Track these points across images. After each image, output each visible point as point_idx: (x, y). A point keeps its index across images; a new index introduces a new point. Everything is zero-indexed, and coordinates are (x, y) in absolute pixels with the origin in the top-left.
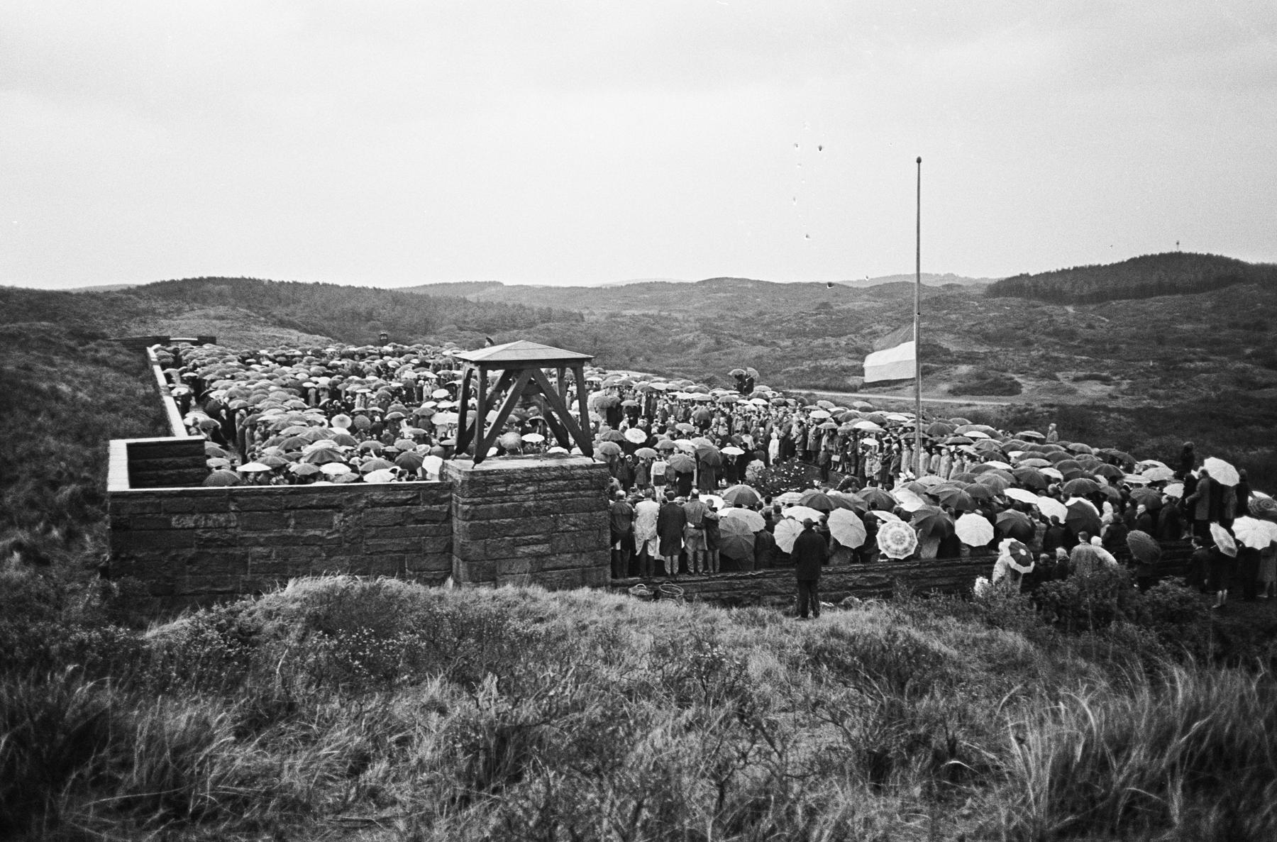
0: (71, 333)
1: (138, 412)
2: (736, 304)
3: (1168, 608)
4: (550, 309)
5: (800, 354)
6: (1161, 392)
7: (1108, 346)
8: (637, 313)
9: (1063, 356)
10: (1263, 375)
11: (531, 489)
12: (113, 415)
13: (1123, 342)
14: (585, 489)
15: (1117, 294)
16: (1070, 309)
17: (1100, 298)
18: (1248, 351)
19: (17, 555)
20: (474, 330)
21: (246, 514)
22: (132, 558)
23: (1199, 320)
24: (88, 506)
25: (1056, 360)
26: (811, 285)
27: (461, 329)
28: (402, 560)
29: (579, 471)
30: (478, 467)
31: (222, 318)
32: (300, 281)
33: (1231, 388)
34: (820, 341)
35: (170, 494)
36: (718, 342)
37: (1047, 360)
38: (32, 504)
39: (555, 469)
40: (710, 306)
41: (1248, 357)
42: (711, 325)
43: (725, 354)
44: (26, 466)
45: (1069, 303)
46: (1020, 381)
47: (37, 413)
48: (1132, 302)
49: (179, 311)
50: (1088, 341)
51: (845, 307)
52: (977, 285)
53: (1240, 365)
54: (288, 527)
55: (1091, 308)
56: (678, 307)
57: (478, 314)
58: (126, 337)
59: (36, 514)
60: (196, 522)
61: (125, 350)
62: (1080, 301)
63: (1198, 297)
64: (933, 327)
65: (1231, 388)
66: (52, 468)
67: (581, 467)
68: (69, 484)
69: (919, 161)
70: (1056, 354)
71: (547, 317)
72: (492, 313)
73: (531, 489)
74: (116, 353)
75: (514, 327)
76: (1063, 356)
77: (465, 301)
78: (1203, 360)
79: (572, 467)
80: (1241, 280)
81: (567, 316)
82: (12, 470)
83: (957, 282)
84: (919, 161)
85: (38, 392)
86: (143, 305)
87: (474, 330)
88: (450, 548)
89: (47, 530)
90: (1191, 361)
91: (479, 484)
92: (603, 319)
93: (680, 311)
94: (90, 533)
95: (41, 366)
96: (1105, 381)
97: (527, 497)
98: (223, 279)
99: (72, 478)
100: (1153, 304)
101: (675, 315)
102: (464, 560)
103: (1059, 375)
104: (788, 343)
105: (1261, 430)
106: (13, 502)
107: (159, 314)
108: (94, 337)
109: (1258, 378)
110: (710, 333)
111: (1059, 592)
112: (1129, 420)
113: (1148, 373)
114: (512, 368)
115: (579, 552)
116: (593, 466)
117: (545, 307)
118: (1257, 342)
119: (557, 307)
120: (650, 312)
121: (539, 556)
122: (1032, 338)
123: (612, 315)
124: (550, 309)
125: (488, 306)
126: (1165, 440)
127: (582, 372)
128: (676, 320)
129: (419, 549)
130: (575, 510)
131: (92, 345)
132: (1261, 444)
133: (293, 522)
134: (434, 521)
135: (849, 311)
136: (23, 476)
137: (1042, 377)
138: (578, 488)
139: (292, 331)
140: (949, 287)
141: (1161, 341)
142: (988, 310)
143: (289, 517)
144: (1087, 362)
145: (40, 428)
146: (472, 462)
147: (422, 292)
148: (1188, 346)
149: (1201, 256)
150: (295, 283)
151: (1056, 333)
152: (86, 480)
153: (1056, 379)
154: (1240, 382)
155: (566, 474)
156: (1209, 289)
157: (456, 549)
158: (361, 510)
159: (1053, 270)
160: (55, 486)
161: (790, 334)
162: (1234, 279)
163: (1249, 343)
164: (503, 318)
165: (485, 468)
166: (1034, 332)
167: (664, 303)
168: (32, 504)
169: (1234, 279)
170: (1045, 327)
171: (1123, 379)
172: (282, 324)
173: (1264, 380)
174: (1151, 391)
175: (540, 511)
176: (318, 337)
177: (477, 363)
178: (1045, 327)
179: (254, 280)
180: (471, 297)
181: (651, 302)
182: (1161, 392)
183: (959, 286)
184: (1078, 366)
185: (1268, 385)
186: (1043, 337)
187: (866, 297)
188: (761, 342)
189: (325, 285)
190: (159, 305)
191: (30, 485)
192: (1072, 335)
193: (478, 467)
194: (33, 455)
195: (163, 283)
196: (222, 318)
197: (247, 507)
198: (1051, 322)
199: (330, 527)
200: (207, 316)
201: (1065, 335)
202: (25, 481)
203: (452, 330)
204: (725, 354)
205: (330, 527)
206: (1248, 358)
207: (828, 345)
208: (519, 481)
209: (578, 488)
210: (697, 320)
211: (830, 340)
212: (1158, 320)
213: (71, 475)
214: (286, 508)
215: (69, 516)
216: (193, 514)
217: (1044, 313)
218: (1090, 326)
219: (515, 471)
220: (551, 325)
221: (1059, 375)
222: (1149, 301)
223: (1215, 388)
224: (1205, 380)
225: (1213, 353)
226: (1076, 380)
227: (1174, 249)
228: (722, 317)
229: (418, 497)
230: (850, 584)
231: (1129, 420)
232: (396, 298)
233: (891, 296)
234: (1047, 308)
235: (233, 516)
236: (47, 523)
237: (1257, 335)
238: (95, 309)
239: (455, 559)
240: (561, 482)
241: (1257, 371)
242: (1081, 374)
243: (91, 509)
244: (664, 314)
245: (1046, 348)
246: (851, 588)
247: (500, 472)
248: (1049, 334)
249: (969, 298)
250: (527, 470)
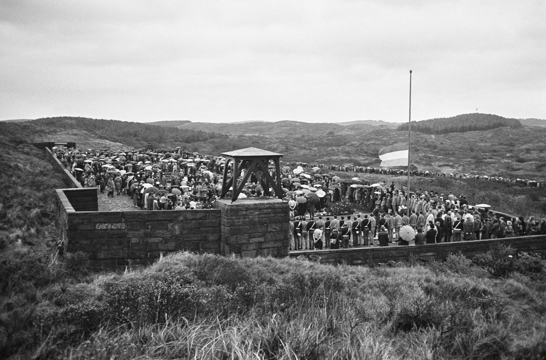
0: (11, 140)
1: (56, 176)
2: (292, 132)
3: (530, 266)
4: (213, 133)
5: (322, 153)
6: (475, 171)
7: (450, 152)
8: (250, 135)
9: (432, 156)
10: (516, 165)
11: (257, 213)
12: (46, 178)
13: (456, 150)
14: (280, 213)
15: (452, 130)
16: (433, 136)
17: (446, 131)
18: (508, 155)
19: (20, 240)
20: (181, 141)
21: (129, 223)
22: (78, 243)
23: (486, 142)
24: (43, 218)
25: (430, 158)
26: (323, 124)
27: (175, 141)
28: (198, 244)
29: (277, 205)
30: (234, 203)
31: (75, 135)
32: (104, 119)
33: (504, 171)
34: (330, 148)
35: (533, 238)
36: (287, 148)
37: (426, 157)
38: (19, 217)
39: (267, 204)
40: (281, 133)
41: (509, 158)
42: (283, 141)
43: (291, 153)
44: (15, 200)
45: (432, 133)
46: (417, 166)
47: (11, 176)
48: (459, 134)
49: (55, 132)
50: (442, 150)
51: (339, 134)
52: (393, 125)
53: (506, 161)
54: (148, 229)
55: (442, 136)
56: (267, 133)
57: (182, 135)
58: (34, 142)
59: (22, 222)
60: (107, 226)
61: (35, 148)
62: (437, 133)
63: (485, 132)
64: (377, 143)
65: (504, 171)
66: (27, 202)
67: (278, 203)
68: (35, 208)
69: (411, 72)
70: (429, 155)
71: (212, 136)
72: (188, 134)
73: (257, 213)
74: (32, 149)
75: (198, 141)
76: (432, 156)
77: (176, 129)
78: (491, 158)
79: (274, 203)
80: (504, 125)
81: (221, 136)
82: (9, 202)
83: (384, 124)
84: (411, 72)
85: (10, 167)
86: (38, 128)
87: (181, 141)
88: (220, 239)
89: (28, 229)
90: (485, 159)
91: (235, 211)
92: (236, 137)
93: (268, 135)
94: (47, 230)
95: (5, 155)
96: (452, 166)
97: (255, 216)
98: (70, 117)
99: (36, 206)
100: (468, 135)
101: (266, 136)
102: (227, 244)
103: (433, 164)
104: (315, 149)
105: (519, 188)
106: (12, 216)
107: (46, 133)
108: (21, 142)
109: (515, 166)
110: (283, 144)
111: (484, 259)
112: (465, 183)
113: (470, 163)
114: (247, 161)
115: (276, 241)
116: (283, 203)
117: (211, 132)
118: (511, 151)
119: (217, 132)
120: (256, 135)
121: (260, 243)
122: (418, 148)
123: (240, 136)
124: (213, 133)
125: (187, 131)
126: (488, 192)
127: (278, 161)
128: (267, 138)
129: (206, 240)
130: (275, 222)
131: (21, 146)
132: (520, 194)
133: (150, 227)
134: (213, 227)
135: (341, 135)
136: (15, 205)
137: (426, 165)
138: (277, 212)
139: (107, 141)
140: (382, 126)
141: (472, 150)
142: (399, 136)
143: (149, 225)
144: (443, 159)
145: (14, 183)
146: (231, 201)
147: (157, 125)
148: (483, 152)
149: (487, 115)
150: (102, 120)
151: (429, 146)
152: (42, 207)
153: (432, 166)
154: (508, 168)
155: (272, 207)
156: (490, 129)
157: (223, 239)
158: (182, 221)
159: (426, 119)
160: (29, 209)
161: (316, 146)
162: (500, 125)
163: (508, 151)
164: (193, 136)
165: (237, 204)
166: (419, 146)
167: (261, 131)
168: (19, 217)
169: (500, 125)
170: (424, 144)
171: (459, 166)
172: (101, 137)
173: (518, 167)
174: (471, 171)
175: (262, 223)
176: (118, 143)
177: (234, 157)
178: (424, 144)
179: (84, 118)
180: (178, 127)
181: (256, 131)
182: (475, 171)
183: (386, 126)
184: (439, 160)
185: (518, 170)
186: (423, 148)
187: (347, 130)
188: (305, 148)
189: (115, 121)
190: (45, 128)
191: (18, 208)
192: (435, 147)
193: (234, 203)
194: (16, 195)
195: (43, 119)
196: (75, 135)
197: (130, 220)
198: (426, 141)
199: (167, 229)
200: (68, 134)
201: (432, 147)
202: (16, 207)
203: (172, 141)
204: (291, 153)
205: (167, 229)
206: (509, 158)
207: (333, 150)
208: (252, 209)
209: (277, 212)
210: (276, 138)
211: (335, 148)
212: (470, 141)
213: (35, 204)
214: (148, 221)
215: (36, 223)
216: (105, 223)
217: (422, 138)
218: (442, 144)
219: (249, 205)
220: (215, 140)
221: (433, 164)
222: (465, 133)
223: (497, 170)
224: (493, 167)
225: (494, 155)
226: (440, 166)
227: (476, 112)
228: (286, 138)
229: (206, 216)
230: (390, 255)
231: (465, 183)
232: (147, 127)
233: (357, 129)
234: (424, 135)
235: (124, 225)
236: (28, 226)
237: (511, 148)
238: (17, 130)
239: (222, 244)
240: (269, 210)
241: (514, 163)
242: (441, 164)
243: (45, 220)
244: (261, 135)
245: (425, 152)
246: (391, 257)
247: (244, 205)
248: (425, 147)
249: (391, 131)
250: (255, 205)
